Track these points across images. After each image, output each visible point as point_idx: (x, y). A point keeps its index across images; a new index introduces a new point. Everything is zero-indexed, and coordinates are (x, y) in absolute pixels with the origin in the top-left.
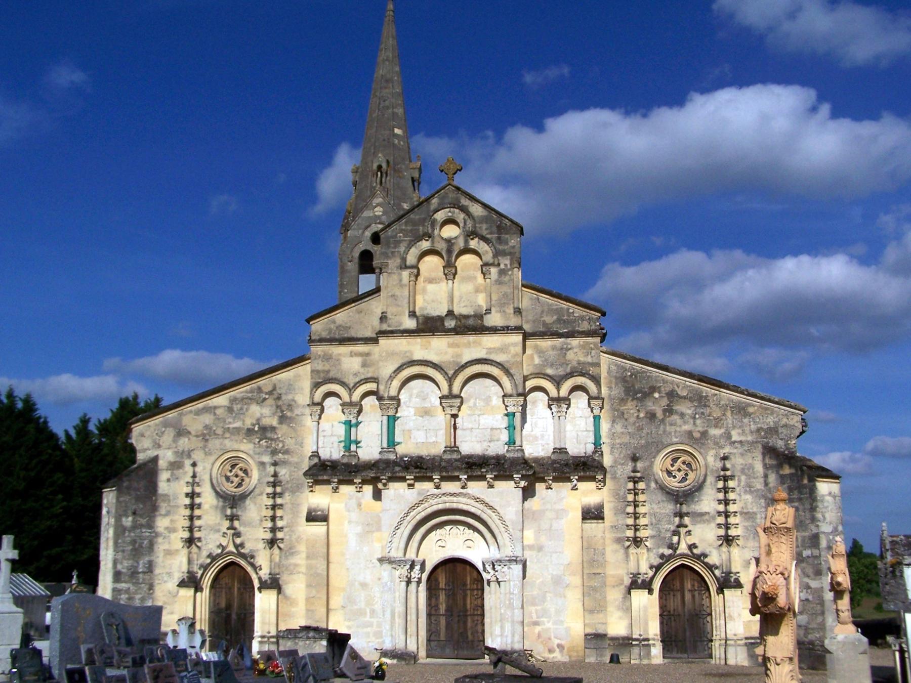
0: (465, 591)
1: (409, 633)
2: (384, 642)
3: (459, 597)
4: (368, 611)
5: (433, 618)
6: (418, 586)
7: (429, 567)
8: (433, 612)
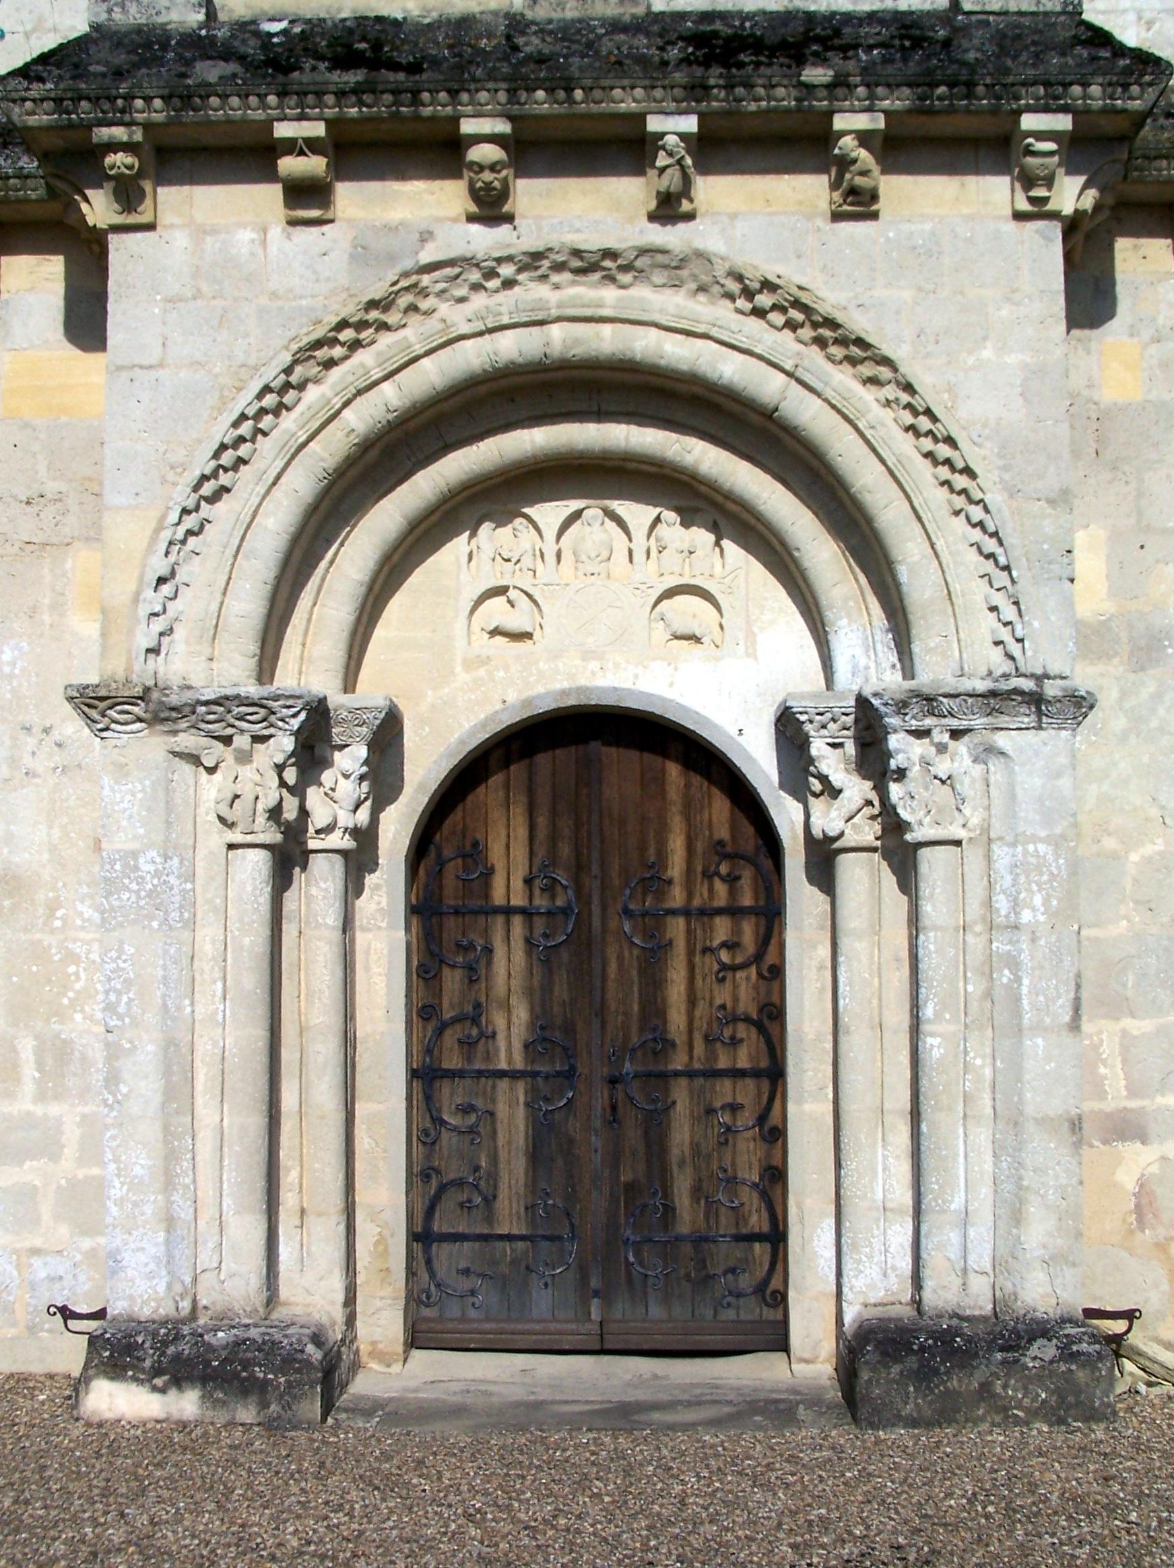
0: (652, 922)
1: (289, 1200)
2: (111, 1264)
3: (618, 963)
4: (27, 1048)
5: (450, 1096)
6: (354, 885)
7: (425, 765)
8: (452, 1060)
